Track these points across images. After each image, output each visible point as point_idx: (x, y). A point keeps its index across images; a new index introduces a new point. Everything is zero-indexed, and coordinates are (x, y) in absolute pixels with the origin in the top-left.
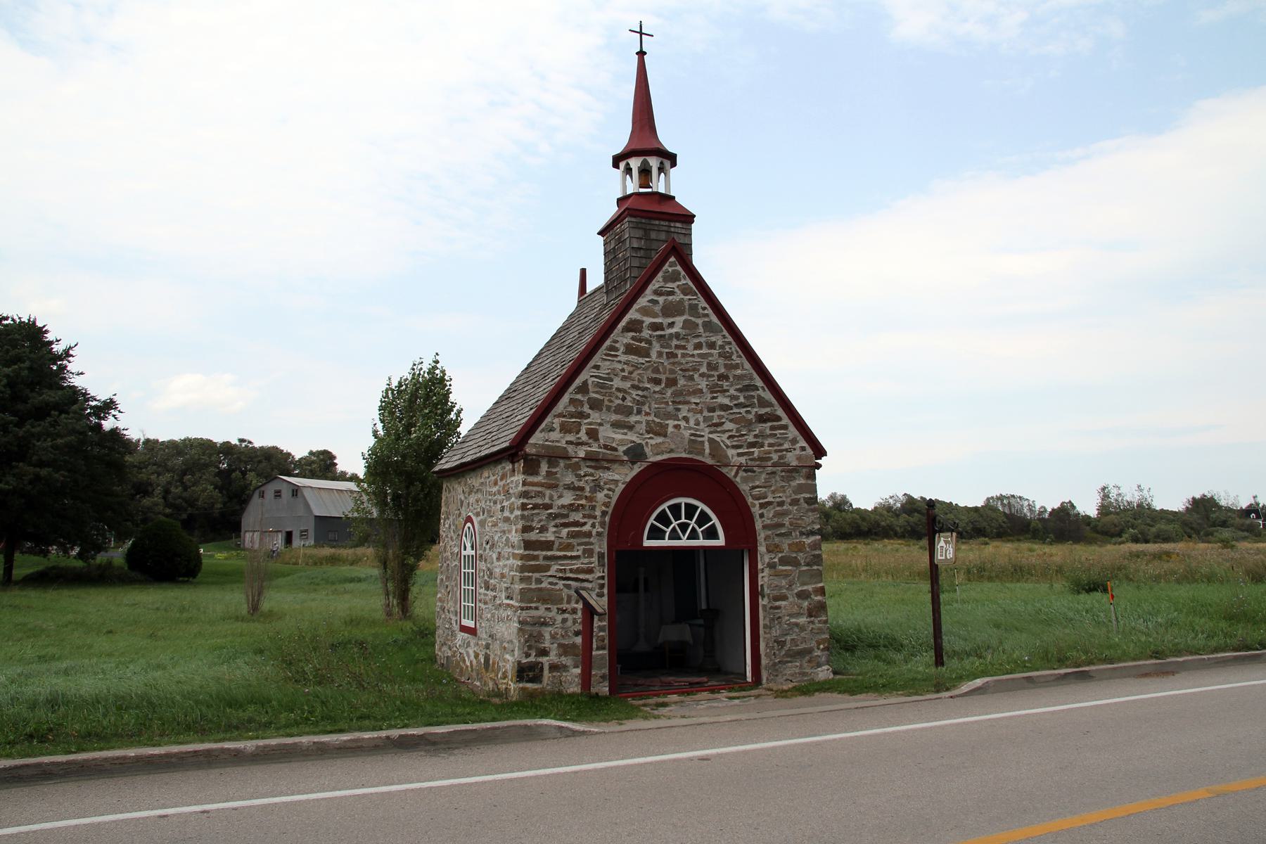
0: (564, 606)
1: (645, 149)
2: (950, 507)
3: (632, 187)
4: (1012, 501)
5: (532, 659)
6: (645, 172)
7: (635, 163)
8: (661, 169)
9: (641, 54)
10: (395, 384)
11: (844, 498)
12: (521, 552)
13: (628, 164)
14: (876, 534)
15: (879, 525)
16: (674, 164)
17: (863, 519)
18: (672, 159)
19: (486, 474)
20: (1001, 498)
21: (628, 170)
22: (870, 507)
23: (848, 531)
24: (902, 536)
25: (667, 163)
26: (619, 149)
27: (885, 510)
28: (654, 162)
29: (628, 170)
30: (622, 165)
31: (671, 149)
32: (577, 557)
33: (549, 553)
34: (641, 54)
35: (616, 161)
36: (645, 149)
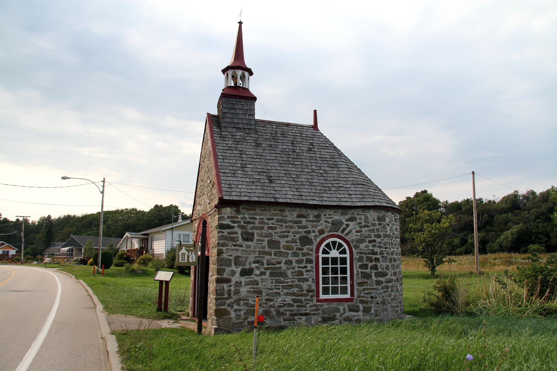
7: (230, 72)
9: (240, 23)
18: (251, 73)
25: (247, 74)
28: (239, 73)
35: (224, 71)
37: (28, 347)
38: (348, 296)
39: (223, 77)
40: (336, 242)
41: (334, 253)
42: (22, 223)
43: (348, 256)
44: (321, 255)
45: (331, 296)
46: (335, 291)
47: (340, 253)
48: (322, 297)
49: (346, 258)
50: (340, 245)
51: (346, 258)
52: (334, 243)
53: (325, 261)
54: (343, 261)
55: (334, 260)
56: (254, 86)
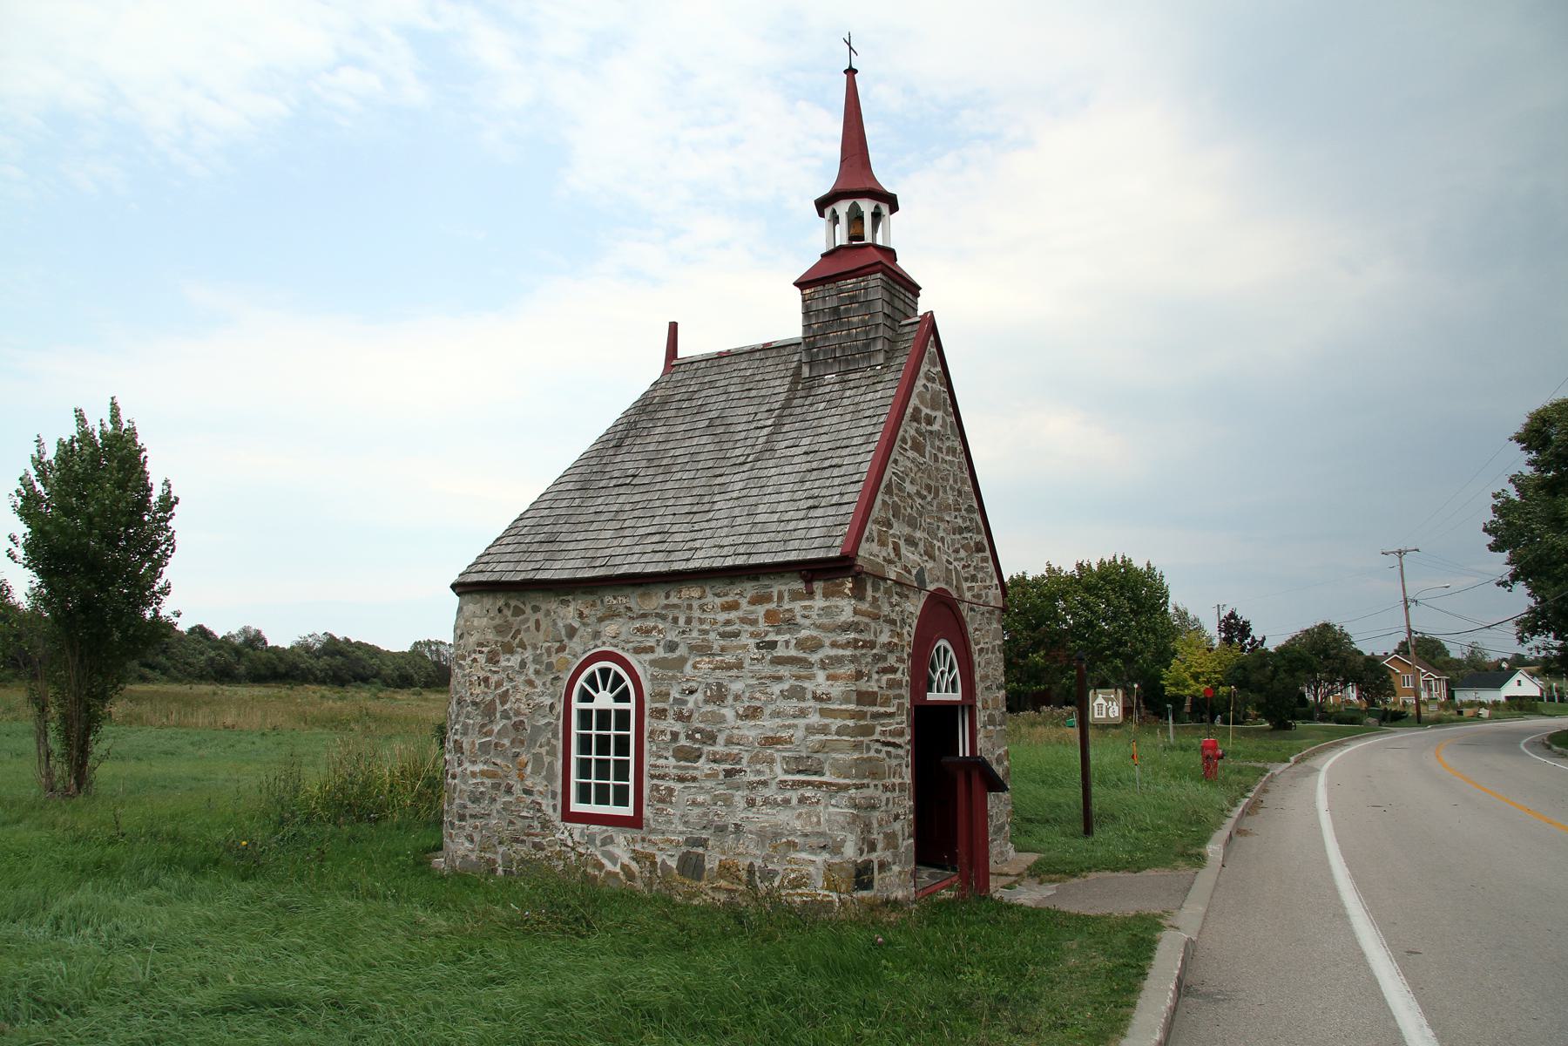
0: (888, 782)
1: (857, 189)
2: (374, 651)
3: (842, 238)
4: (442, 648)
5: (865, 857)
6: (856, 218)
7: (843, 208)
8: (877, 216)
9: (851, 72)
10: (51, 454)
11: (258, 632)
12: (852, 707)
13: (834, 211)
14: (293, 678)
15: (297, 668)
16: (894, 208)
17: (281, 660)
18: (892, 203)
19: (685, 593)
20: (429, 643)
21: (835, 219)
22: (287, 646)
23: (263, 671)
24: (323, 682)
25: (885, 209)
26: (825, 189)
27: (304, 648)
28: (867, 207)
29: (835, 219)
30: (828, 212)
31: (889, 189)
32: (891, 715)
33: (875, 709)
34: (851, 72)
35: (822, 204)
36: (857, 189)
37: (1374, 982)
38: (628, 811)
39: (823, 224)
40: (609, 670)
41: (604, 700)
42: (35, 608)
43: (631, 706)
44: (576, 705)
45: (593, 808)
46: (602, 799)
47: (617, 699)
48: (576, 807)
49: (628, 712)
50: (618, 680)
51: (628, 712)
52: (605, 672)
53: (585, 716)
54: (623, 717)
55: (604, 715)
56: (906, 237)
